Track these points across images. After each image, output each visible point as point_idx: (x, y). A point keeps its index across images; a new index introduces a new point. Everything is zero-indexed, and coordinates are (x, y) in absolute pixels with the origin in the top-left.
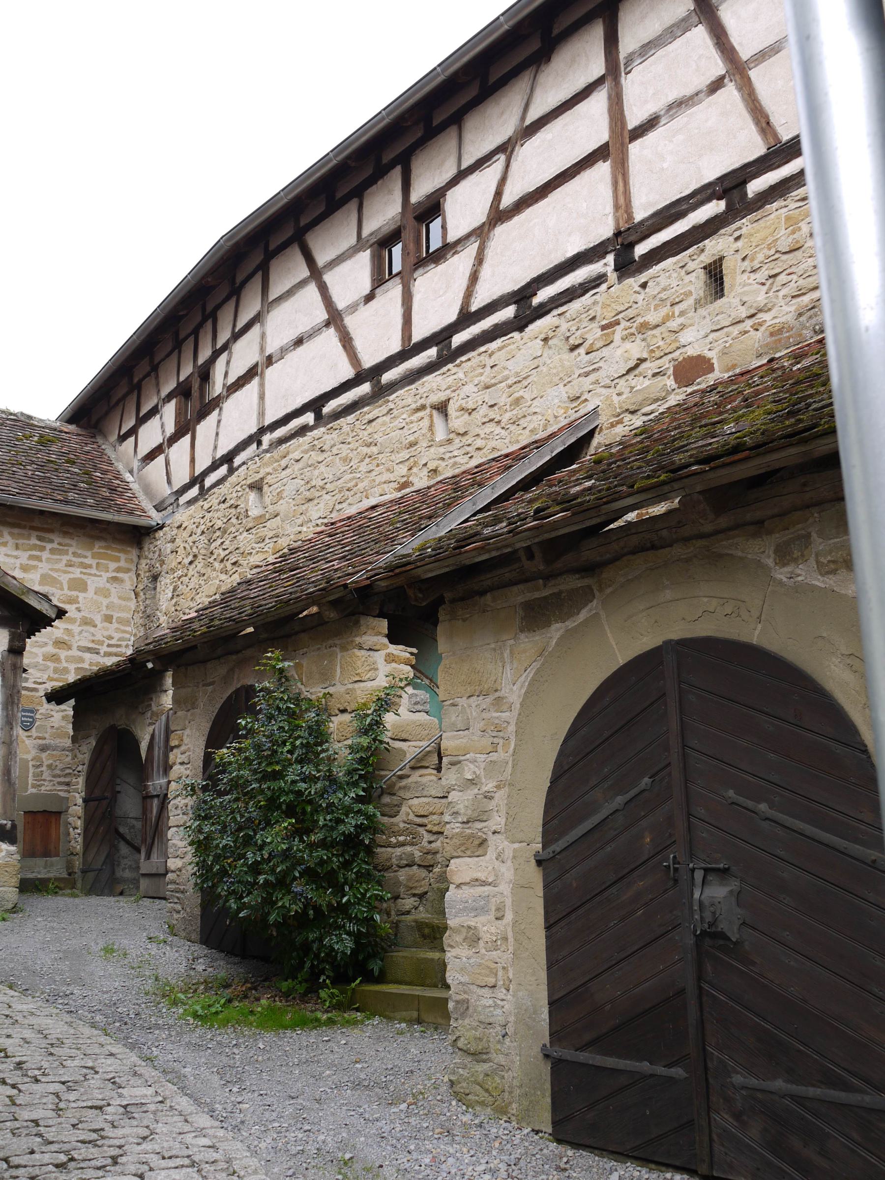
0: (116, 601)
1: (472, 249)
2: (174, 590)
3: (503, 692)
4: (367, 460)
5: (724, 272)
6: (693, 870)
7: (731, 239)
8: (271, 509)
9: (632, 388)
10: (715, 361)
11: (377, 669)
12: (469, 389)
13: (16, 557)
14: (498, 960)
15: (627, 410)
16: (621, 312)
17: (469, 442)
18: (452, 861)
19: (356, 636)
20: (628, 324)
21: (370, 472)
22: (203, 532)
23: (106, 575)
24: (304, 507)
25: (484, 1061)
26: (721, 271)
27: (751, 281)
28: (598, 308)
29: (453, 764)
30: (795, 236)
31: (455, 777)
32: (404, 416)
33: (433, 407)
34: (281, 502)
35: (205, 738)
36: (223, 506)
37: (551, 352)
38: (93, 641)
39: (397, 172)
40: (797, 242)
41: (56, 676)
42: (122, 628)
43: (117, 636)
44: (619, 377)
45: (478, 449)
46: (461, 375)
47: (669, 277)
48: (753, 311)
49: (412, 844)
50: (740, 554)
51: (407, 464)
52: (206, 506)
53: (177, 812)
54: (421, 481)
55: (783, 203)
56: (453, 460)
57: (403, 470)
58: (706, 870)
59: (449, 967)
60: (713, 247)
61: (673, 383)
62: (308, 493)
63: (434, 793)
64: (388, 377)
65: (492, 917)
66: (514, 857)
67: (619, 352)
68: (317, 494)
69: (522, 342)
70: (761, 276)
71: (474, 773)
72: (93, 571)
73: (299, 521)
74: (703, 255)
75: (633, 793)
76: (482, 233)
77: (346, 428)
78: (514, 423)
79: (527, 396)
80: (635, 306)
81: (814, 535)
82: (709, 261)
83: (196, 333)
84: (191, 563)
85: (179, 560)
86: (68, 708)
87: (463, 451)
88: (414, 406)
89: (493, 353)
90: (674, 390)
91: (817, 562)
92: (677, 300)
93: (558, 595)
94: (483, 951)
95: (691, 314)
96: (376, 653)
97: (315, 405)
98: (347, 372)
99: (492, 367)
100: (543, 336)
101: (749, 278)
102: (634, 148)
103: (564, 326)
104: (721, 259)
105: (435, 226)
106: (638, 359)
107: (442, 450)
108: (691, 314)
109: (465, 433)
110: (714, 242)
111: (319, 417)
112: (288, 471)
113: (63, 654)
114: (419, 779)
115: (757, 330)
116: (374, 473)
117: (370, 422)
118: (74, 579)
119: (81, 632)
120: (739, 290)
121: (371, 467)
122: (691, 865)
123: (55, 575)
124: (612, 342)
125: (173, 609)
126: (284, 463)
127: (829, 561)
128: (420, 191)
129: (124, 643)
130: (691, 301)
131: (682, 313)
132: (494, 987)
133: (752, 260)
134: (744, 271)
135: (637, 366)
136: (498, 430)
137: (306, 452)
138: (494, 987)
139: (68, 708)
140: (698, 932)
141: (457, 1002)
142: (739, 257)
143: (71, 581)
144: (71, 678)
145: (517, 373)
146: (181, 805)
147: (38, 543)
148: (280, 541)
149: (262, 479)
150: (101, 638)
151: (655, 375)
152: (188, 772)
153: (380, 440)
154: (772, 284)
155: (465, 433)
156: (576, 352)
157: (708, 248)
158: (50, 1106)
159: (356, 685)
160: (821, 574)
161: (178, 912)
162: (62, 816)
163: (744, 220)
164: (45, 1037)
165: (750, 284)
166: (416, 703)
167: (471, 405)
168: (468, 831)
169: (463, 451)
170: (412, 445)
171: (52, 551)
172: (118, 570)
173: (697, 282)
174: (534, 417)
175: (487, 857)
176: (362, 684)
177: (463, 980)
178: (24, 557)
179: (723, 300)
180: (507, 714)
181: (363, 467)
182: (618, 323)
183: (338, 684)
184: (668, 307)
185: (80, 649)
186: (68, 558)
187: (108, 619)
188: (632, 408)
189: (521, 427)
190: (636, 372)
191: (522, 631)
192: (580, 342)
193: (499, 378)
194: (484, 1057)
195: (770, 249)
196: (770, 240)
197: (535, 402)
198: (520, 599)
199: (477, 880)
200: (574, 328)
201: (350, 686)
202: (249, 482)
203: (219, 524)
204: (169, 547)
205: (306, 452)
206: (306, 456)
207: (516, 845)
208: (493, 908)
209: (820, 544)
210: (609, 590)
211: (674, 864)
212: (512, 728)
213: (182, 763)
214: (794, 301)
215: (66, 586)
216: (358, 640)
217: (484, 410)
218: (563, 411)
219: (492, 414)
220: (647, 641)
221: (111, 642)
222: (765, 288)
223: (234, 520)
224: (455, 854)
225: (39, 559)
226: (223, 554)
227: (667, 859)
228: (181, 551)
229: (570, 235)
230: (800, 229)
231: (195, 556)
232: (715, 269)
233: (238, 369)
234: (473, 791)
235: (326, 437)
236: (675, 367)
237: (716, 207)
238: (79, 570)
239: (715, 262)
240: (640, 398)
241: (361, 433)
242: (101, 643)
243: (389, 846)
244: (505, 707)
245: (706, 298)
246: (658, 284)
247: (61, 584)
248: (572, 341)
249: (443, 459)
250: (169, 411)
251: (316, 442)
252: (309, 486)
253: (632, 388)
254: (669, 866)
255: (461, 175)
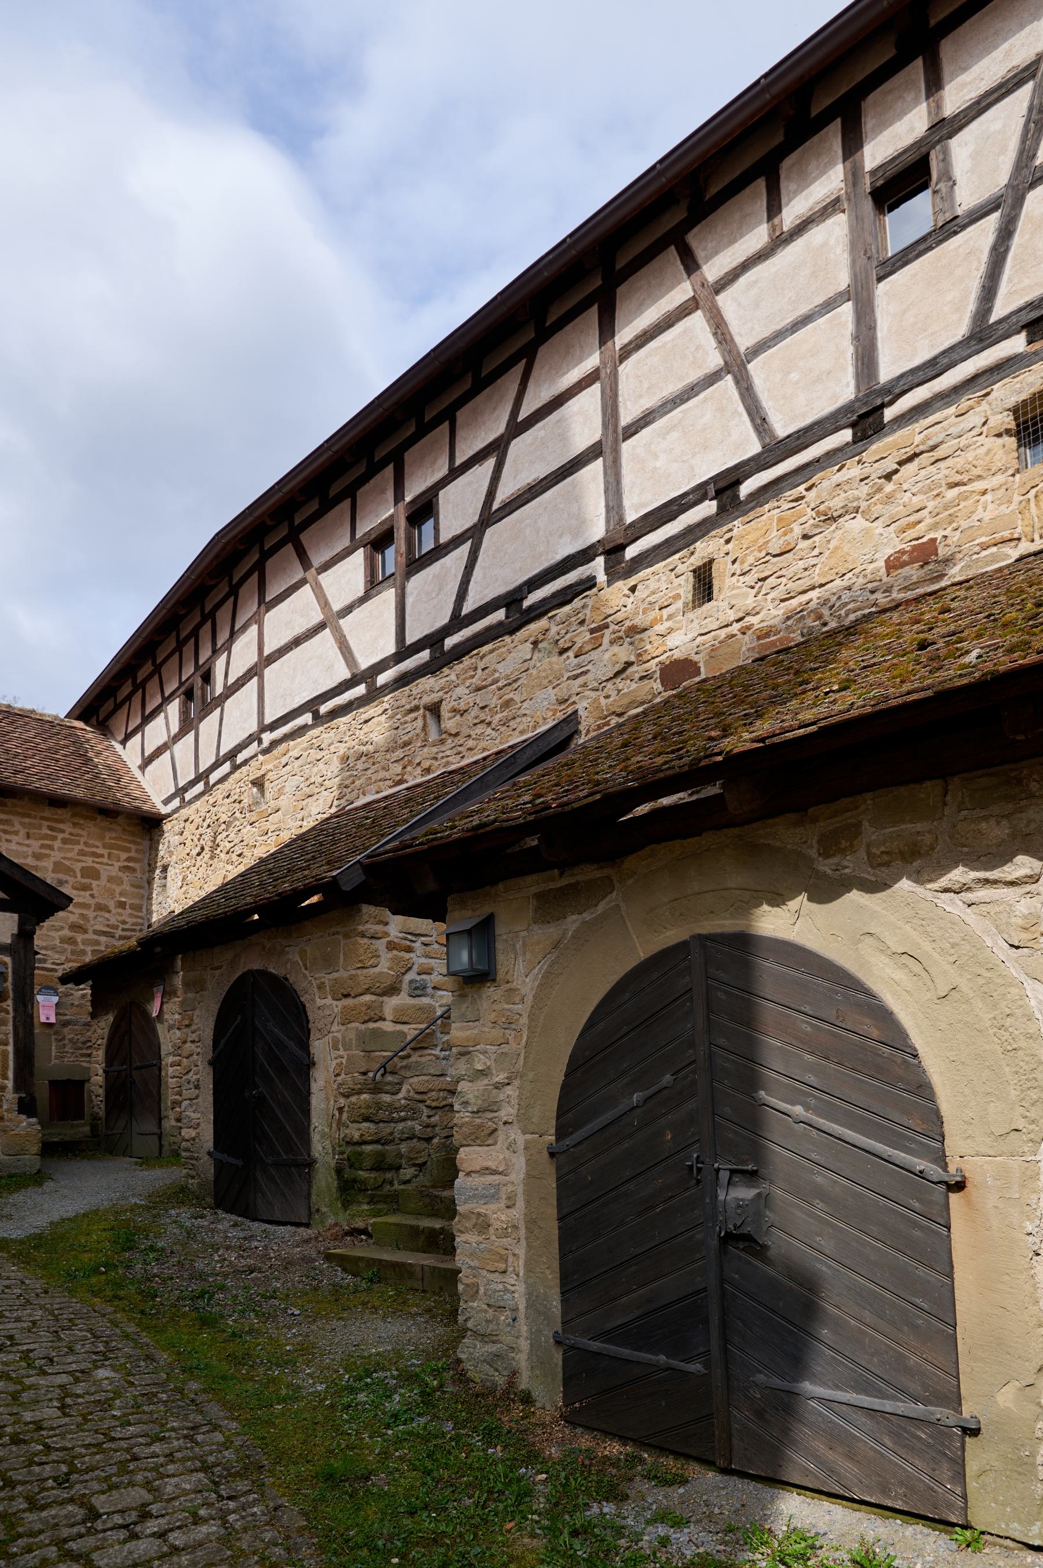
0: (128, 888)
1: (465, 548)
2: (184, 879)
3: (515, 983)
4: (364, 758)
5: (714, 575)
6: (718, 1170)
7: (722, 541)
8: (273, 804)
9: (619, 691)
10: (701, 665)
11: (379, 956)
12: (461, 691)
13: (28, 846)
14: (509, 1247)
15: (614, 713)
16: (610, 615)
17: (461, 742)
18: (461, 1149)
19: (359, 924)
20: (617, 627)
21: (366, 770)
22: (209, 826)
23: (117, 865)
24: (304, 803)
25: (494, 1342)
26: (710, 575)
27: (740, 584)
28: (588, 611)
29: (462, 1054)
30: (786, 538)
31: (465, 1067)
32: (399, 716)
33: (426, 708)
34: (282, 797)
35: (214, 1018)
36: (227, 801)
37: (540, 655)
38: (108, 926)
39: (389, 471)
40: (789, 544)
41: (74, 957)
42: (136, 913)
43: (131, 920)
44: (607, 680)
45: (470, 749)
46: (453, 677)
47: (659, 580)
48: (741, 615)
49: (413, 1119)
50: (778, 844)
51: (401, 763)
52: (211, 801)
53: (189, 1086)
54: (415, 778)
55: (776, 504)
56: (445, 760)
57: (397, 768)
58: (733, 1172)
59: (458, 1251)
60: (704, 549)
61: (660, 686)
62: (307, 789)
63: (432, 1071)
64: (382, 679)
65: (502, 1205)
66: (525, 1148)
67: (607, 655)
68: (317, 790)
69: (513, 645)
70: (750, 579)
71: (485, 1063)
72: (105, 860)
73: (300, 816)
74: (693, 557)
75: (652, 1090)
76: (475, 534)
77: (343, 728)
78: (504, 724)
79: (517, 698)
80: (624, 609)
81: (866, 824)
82: (700, 563)
83: (195, 634)
84: (199, 854)
85: (187, 851)
86: (85, 990)
87: (455, 751)
88: (408, 707)
89: (484, 656)
90: (660, 693)
91: (869, 854)
92: (666, 604)
93: (574, 886)
94: (493, 1238)
95: (680, 617)
96: (378, 942)
97: (311, 705)
98: (343, 673)
99: (483, 670)
100: (532, 639)
101: (738, 581)
102: (626, 447)
103: (554, 629)
104: (711, 562)
105: (428, 527)
106: (626, 663)
107: (435, 750)
108: (680, 617)
109: (457, 734)
110: (704, 544)
111: (316, 716)
112: (288, 767)
113: (80, 937)
114: (419, 1059)
115: (744, 633)
116: (370, 771)
117: (366, 722)
118: (87, 867)
119: (95, 918)
120: (726, 593)
121: (367, 765)
122: (716, 1165)
123: (68, 863)
124: (600, 645)
125: (183, 897)
126: (284, 760)
127: (882, 852)
128: (413, 490)
129: (138, 928)
130: (679, 604)
131: (670, 617)
132: (505, 1272)
133: (742, 563)
134: (733, 574)
135: (623, 670)
136: (489, 731)
137: (306, 749)
138: (505, 1272)
139: (85, 990)
140: (723, 1234)
141: (467, 1285)
142: (730, 558)
143: (83, 869)
144: (88, 958)
145: (508, 676)
146: (193, 1080)
147: (49, 832)
148: (282, 834)
149: (263, 775)
150: (116, 923)
151: (642, 678)
152: (199, 1050)
153: (375, 739)
154: (761, 587)
155: (457, 734)
156: (565, 656)
157: (698, 550)
158: (56, 1404)
159: (359, 972)
160: (872, 866)
161: (193, 1177)
162: (86, 1085)
163: (735, 523)
164: (57, 1320)
165: (739, 588)
166: (416, 989)
167: (462, 706)
168: (478, 1121)
169: (455, 751)
170: (406, 744)
171: (65, 841)
172: (129, 859)
173: (685, 586)
174: (524, 719)
175: (498, 1147)
176: (365, 971)
177: (472, 1264)
178: (35, 845)
179: (712, 603)
180: (520, 1006)
181: (360, 765)
182: (607, 626)
183: (342, 970)
184: (657, 610)
185: (96, 932)
186: (80, 847)
187: (122, 905)
188: (619, 710)
189: (511, 729)
190: (624, 676)
191: (535, 923)
192: (570, 645)
193: (490, 680)
194: (495, 1338)
195: (760, 551)
196: (762, 541)
197: (525, 705)
198: (534, 890)
199: (487, 1169)
200: (563, 632)
201: (354, 972)
202: (251, 779)
203: (224, 818)
204: (177, 839)
205: (306, 749)
206: (305, 754)
207: (529, 1137)
208: (504, 1197)
209: (873, 833)
210: (631, 881)
211: (697, 1163)
212: (524, 1020)
213: (193, 1042)
214: (782, 604)
215: (79, 875)
216: (361, 928)
217: (475, 712)
218: (551, 713)
219: (482, 717)
220: (672, 935)
221: (125, 927)
222: (754, 591)
223: (238, 815)
224: (465, 1143)
225: (51, 848)
226: (229, 846)
227: (690, 1158)
228: (188, 842)
229: (560, 537)
230: (792, 530)
231: (202, 849)
232: (705, 572)
233: (237, 671)
234: (482, 1083)
235: (324, 735)
236: (661, 670)
237: (709, 508)
238: (91, 859)
239: (704, 565)
240: (626, 701)
241: (357, 732)
242: (116, 927)
243: (391, 1121)
244: (517, 999)
245: (693, 601)
246: (647, 587)
247: (74, 872)
248: (562, 644)
249: (436, 759)
250: (174, 708)
251: (314, 741)
252: (308, 783)
253: (619, 691)
254: (692, 1166)
255: (455, 472)
